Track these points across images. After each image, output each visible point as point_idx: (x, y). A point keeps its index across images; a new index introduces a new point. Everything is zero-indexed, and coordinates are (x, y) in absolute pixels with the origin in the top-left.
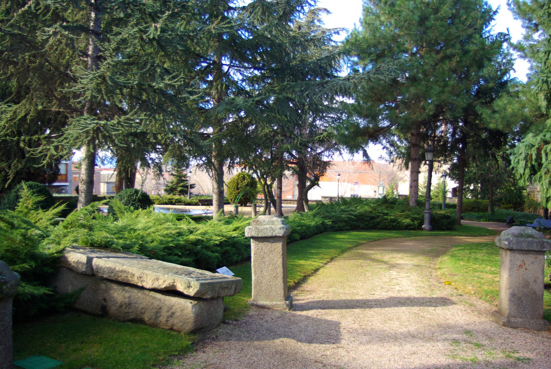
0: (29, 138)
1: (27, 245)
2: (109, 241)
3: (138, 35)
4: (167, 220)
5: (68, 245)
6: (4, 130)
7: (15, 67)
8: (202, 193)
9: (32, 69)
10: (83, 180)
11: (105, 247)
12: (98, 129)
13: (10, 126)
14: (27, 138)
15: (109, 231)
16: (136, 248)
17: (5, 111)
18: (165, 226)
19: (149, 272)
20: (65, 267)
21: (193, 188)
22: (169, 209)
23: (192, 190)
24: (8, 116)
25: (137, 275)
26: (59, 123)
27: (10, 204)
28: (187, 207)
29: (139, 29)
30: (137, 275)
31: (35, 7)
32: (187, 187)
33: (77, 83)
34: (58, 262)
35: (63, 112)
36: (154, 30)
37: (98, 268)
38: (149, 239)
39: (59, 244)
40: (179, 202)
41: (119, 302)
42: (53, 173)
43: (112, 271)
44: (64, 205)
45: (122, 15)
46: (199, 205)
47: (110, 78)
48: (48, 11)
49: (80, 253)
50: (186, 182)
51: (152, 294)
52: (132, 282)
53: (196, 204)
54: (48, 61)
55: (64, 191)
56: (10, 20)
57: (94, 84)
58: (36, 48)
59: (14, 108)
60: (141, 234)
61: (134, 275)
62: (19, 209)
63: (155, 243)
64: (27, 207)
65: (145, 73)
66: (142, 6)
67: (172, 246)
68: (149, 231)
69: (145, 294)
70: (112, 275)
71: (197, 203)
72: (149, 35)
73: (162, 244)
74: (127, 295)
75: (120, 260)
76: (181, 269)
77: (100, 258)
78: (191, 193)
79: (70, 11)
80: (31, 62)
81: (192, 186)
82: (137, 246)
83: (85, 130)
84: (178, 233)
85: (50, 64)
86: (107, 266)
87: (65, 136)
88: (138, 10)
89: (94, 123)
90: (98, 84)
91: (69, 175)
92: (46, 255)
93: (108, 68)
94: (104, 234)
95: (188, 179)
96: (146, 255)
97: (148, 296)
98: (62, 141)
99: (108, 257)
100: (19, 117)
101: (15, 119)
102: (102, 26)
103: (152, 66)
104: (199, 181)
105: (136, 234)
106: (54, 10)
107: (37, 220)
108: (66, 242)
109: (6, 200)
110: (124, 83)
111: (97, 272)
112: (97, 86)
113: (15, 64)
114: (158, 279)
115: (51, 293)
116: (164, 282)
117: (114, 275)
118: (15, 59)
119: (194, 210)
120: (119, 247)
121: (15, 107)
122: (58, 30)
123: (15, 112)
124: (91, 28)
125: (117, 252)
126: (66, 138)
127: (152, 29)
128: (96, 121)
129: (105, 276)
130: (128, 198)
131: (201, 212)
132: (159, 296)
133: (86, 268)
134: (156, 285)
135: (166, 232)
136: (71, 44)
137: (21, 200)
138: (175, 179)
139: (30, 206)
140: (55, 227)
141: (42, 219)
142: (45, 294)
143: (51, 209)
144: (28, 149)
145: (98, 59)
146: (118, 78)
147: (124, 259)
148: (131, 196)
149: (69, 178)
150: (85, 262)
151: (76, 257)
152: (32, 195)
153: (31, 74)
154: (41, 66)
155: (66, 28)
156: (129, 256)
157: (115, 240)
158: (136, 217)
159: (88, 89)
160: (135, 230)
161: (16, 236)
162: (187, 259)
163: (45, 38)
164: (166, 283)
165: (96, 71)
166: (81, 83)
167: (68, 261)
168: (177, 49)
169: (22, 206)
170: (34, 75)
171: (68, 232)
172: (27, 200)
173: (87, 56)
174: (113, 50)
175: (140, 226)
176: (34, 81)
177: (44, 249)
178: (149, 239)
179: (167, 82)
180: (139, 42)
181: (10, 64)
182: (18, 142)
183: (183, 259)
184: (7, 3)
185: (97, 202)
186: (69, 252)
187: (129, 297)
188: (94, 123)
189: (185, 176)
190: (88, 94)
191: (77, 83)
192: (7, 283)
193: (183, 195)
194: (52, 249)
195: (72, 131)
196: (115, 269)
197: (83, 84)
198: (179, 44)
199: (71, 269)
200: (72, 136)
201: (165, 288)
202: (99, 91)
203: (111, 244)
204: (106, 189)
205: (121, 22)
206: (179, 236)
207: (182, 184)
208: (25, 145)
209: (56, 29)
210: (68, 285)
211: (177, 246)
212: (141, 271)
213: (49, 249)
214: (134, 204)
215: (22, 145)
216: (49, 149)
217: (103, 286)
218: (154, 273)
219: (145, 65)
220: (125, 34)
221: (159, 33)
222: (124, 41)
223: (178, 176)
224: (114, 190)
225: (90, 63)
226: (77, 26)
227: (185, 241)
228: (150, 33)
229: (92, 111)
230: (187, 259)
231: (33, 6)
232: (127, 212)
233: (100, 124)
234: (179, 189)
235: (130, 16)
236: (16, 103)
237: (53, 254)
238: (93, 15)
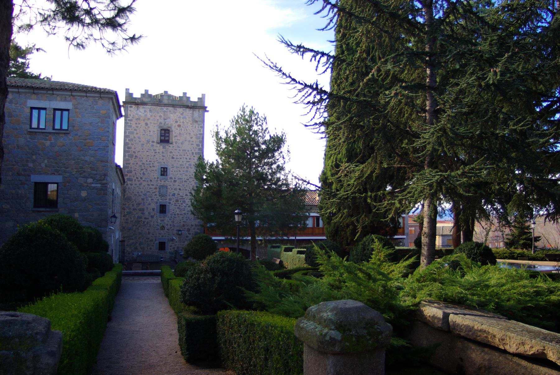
0: (374, 194)
1: (386, 296)
2: (463, 297)
3: (477, 83)
4: (521, 278)
5: (424, 299)
6: (353, 188)
7: (361, 130)
8: (548, 246)
9: (376, 130)
10: (425, 233)
11: (459, 302)
12: (442, 181)
13: (358, 184)
14: (373, 195)
15: (462, 286)
16: (492, 306)
17: (353, 170)
18: (521, 283)
19: (513, 334)
20: (420, 321)
21: (538, 241)
22: (518, 265)
23: (537, 244)
24: (357, 175)
25: (498, 336)
26: (397, 178)
27: (358, 256)
28: (530, 262)
29: (476, 76)
30: (498, 336)
31: (377, 74)
32: (531, 240)
33: (420, 138)
34: (413, 315)
35: (405, 168)
36: (493, 75)
37: (455, 325)
38: (504, 297)
39: (414, 297)
40: (522, 257)
41: (478, 364)
42: (396, 227)
43: (470, 329)
44: (414, 257)
45: (458, 67)
46: (546, 260)
47: (451, 129)
48: (388, 76)
49: (435, 307)
50: (529, 235)
51: (516, 359)
52: (493, 344)
53: (542, 259)
54: (389, 121)
55: (401, 244)
56: (357, 90)
57: (435, 137)
58: (378, 110)
59: (361, 167)
60: (495, 291)
61: (495, 336)
62: (373, 261)
63: (512, 302)
64: (379, 260)
65: (486, 121)
66: (477, 53)
67: (530, 306)
68: (504, 288)
69: (508, 359)
70: (471, 333)
71: (544, 258)
72: (488, 81)
73: (520, 304)
74: (487, 357)
75: (477, 318)
76: (548, 334)
77: (457, 314)
78: (535, 247)
79: (406, 72)
80: (375, 124)
81: (537, 239)
82: (493, 304)
83: (429, 182)
84: (535, 292)
85: (391, 123)
86: (465, 324)
87: (408, 190)
88: (473, 58)
89: (438, 175)
90: (438, 138)
91: (405, 228)
92: (403, 307)
93: (448, 120)
94: (459, 290)
95: (532, 231)
96: (503, 315)
97: (511, 361)
98: (406, 195)
99: (465, 314)
100: (367, 175)
101: (362, 177)
102: (438, 80)
103: (494, 112)
104: (544, 233)
105: (489, 291)
106: (393, 74)
107: (389, 271)
108: (421, 296)
109: (355, 252)
110: (464, 133)
111: (454, 328)
112: (438, 139)
113: (362, 127)
114: (523, 344)
115: (408, 345)
116: (532, 346)
117: (472, 334)
118: (361, 123)
119: (539, 266)
120: (475, 304)
121: (361, 166)
122: (398, 91)
123: (362, 171)
124: (427, 85)
125: (472, 310)
126: (409, 193)
127: (491, 74)
128: (439, 173)
129: (462, 334)
130: (469, 251)
131: (548, 268)
132: (524, 363)
133: (442, 324)
134: (521, 350)
135: (522, 290)
136: (410, 103)
137: (374, 253)
138: (516, 232)
139: (382, 259)
140: (405, 279)
141: (394, 271)
142: (403, 346)
143: (401, 262)
144: (375, 204)
145: (436, 113)
146: (458, 129)
147: (481, 318)
148: (472, 249)
149: (406, 232)
150: (441, 317)
151: (432, 311)
152: (383, 247)
153: (376, 135)
154: (384, 126)
155: (405, 88)
156: (483, 314)
157: (469, 296)
158: (485, 273)
159: (429, 143)
160: (488, 287)
161: (378, 287)
162: (549, 323)
163: (387, 100)
164: (534, 349)
165: (436, 124)
166: (423, 137)
167: (424, 315)
168: (518, 90)
169: (375, 259)
170: (379, 135)
171: (423, 285)
172: (379, 252)
173: (425, 111)
174: (452, 101)
175: (493, 282)
176: (377, 140)
177: (400, 301)
178: (504, 297)
179: (511, 127)
180: (477, 90)
181: (358, 128)
182: (366, 198)
183: (545, 323)
184: (354, 75)
185: (449, 256)
186: (424, 306)
187: (489, 359)
188: (438, 175)
189: (528, 227)
190: (429, 147)
191: (420, 138)
192: (382, 333)
193: (526, 249)
194: (407, 302)
195: (414, 183)
196: (473, 327)
197: (425, 138)
198: (521, 85)
199: (426, 322)
200: (416, 190)
201: (532, 354)
202: (440, 144)
203: (465, 301)
204: (441, 242)
205: (461, 72)
206: (537, 296)
207: (524, 237)
208: (371, 201)
209: (397, 90)
210: (424, 340)
211: (537, 307)
212: (503, 332)
213: (405, 301)
214: (476, 258)
215: (369, 201)
216: (394, 203)
217: (459, 344)
218: (519, 337)
219: (487, 111)
220: (463, 84)
221: (498, 77)
222: (462, 91)
223: (519, 228)
224: (451, 243)
225: (428, 118)
226: (414, 85)
227: (545, 301)
228: (490, 79)
229: (433, 165)
230: (549, 323)
231: (375, 74)
232: (475, 267)
233: (444, 176)
234: (522, 242)
235: (466, 65)
236: (362, 163)
237: (409, 306)
238: (428, 72)
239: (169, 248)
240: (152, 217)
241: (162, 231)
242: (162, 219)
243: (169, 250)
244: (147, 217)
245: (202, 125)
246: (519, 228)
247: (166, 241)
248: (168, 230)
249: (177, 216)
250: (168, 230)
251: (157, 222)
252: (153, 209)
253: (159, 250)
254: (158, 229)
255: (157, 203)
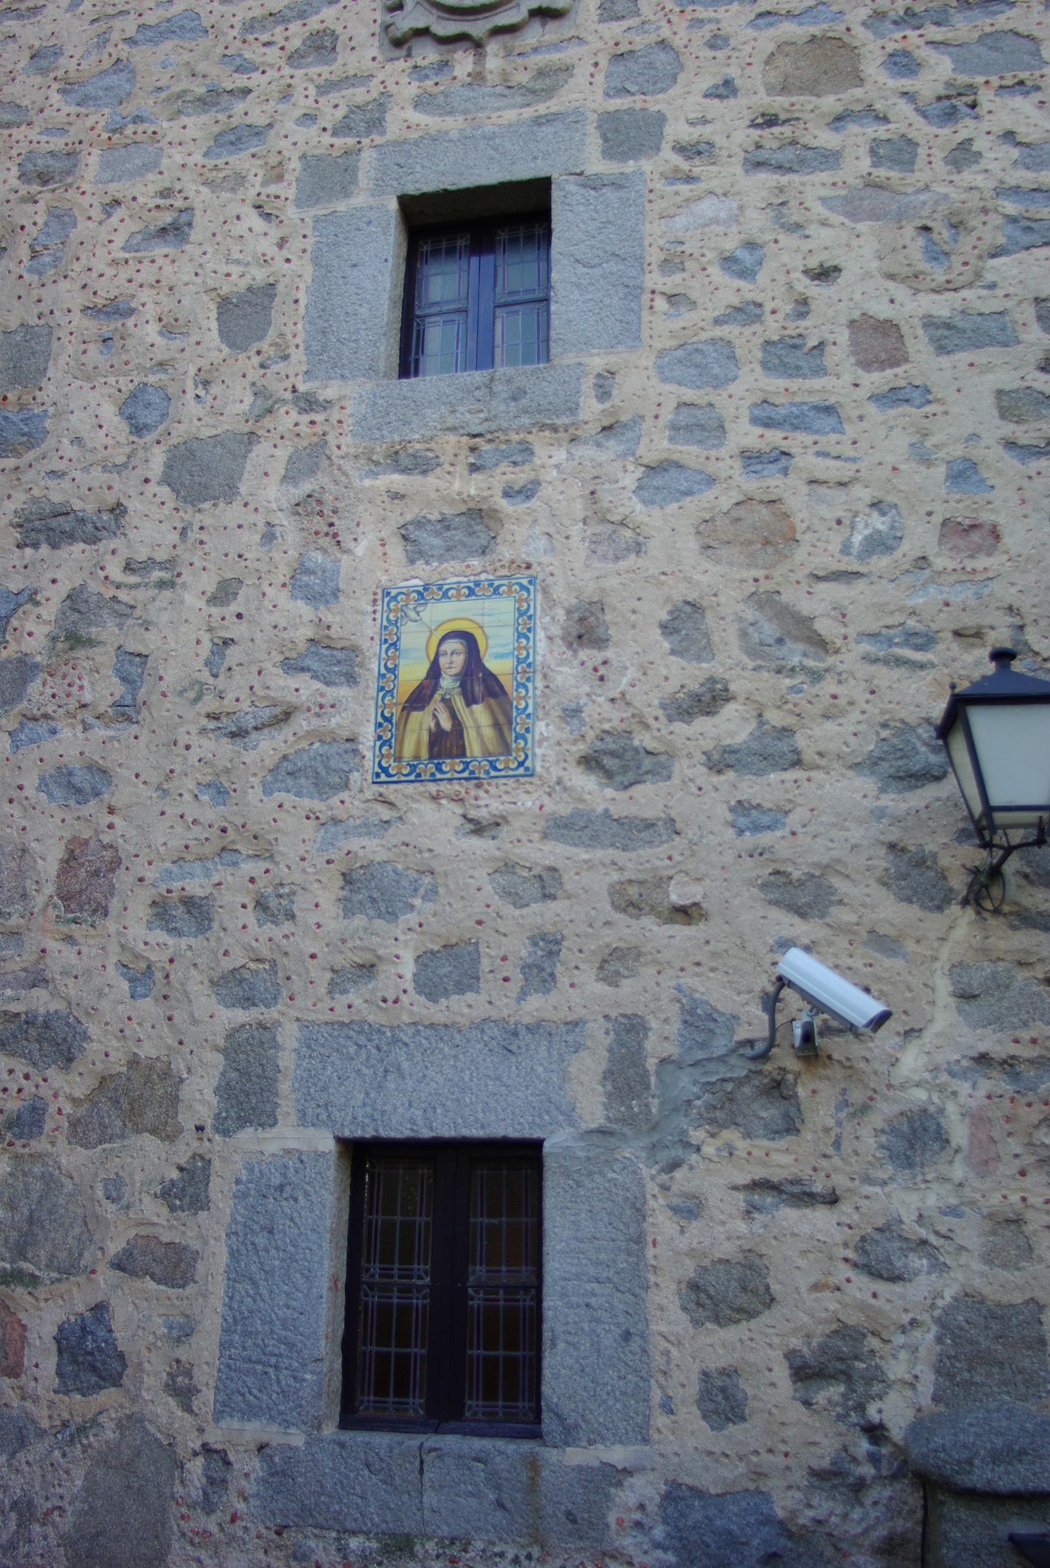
223: (902, 1087)
239: (685, 1348)
240: (200, 477)
241: (431, 821)
242: (455, 485)
243: (686, 1443)
244: (80, 491)
245: (525, 1272)
246: (902, 1087)
247: (563, 1106)
248: (613, 759)
249: (844, 381)
250: (613, 759)
251: (316, 588)
252: (245, 313)
253: (351, 1417)
254: (316, 773)
255: (329, 176)
